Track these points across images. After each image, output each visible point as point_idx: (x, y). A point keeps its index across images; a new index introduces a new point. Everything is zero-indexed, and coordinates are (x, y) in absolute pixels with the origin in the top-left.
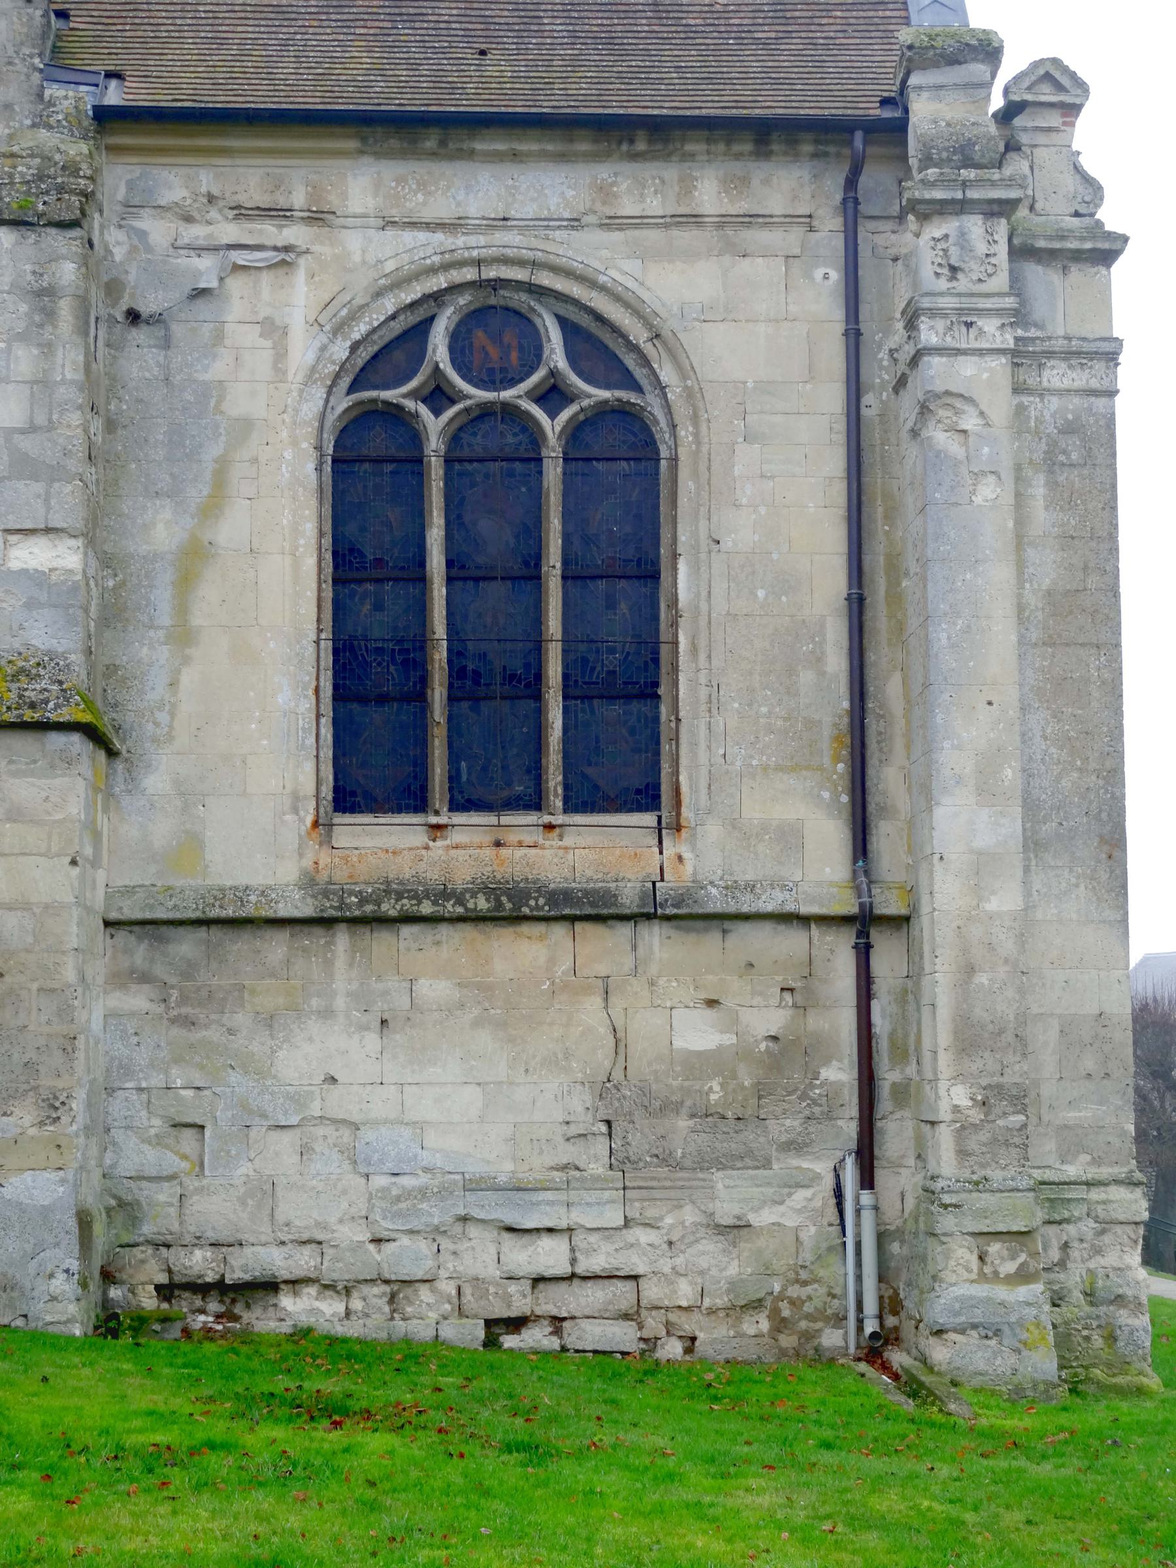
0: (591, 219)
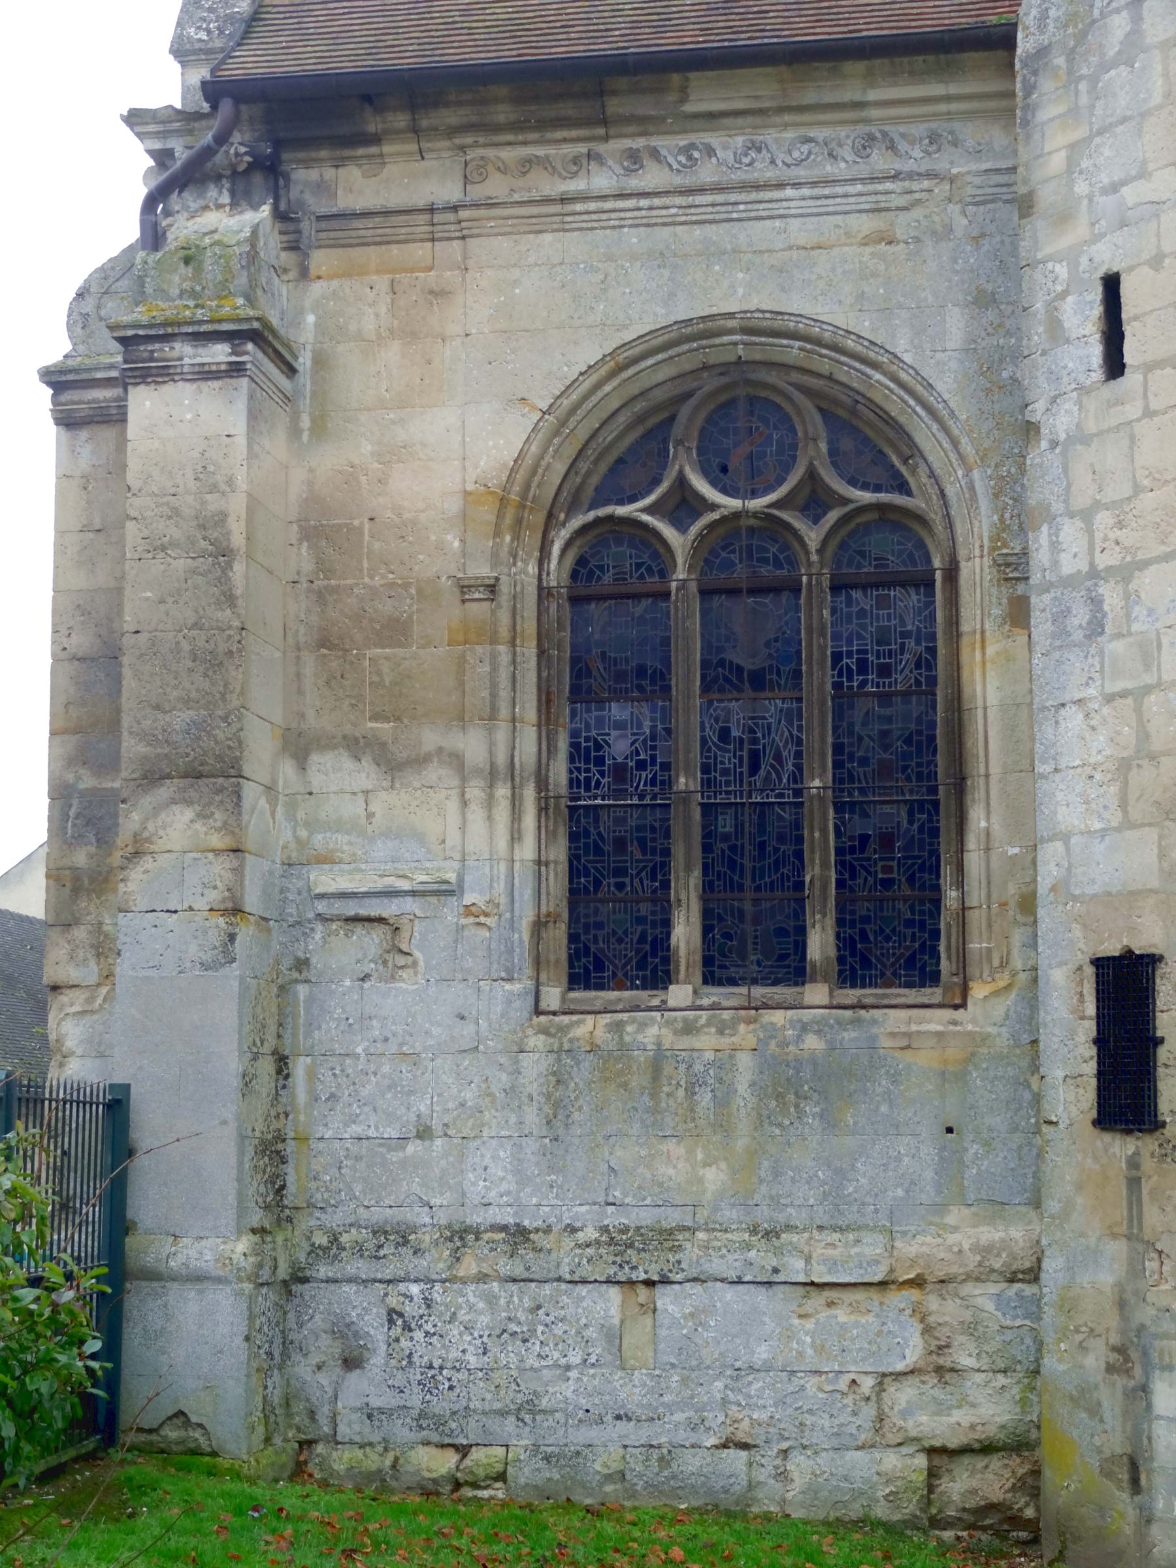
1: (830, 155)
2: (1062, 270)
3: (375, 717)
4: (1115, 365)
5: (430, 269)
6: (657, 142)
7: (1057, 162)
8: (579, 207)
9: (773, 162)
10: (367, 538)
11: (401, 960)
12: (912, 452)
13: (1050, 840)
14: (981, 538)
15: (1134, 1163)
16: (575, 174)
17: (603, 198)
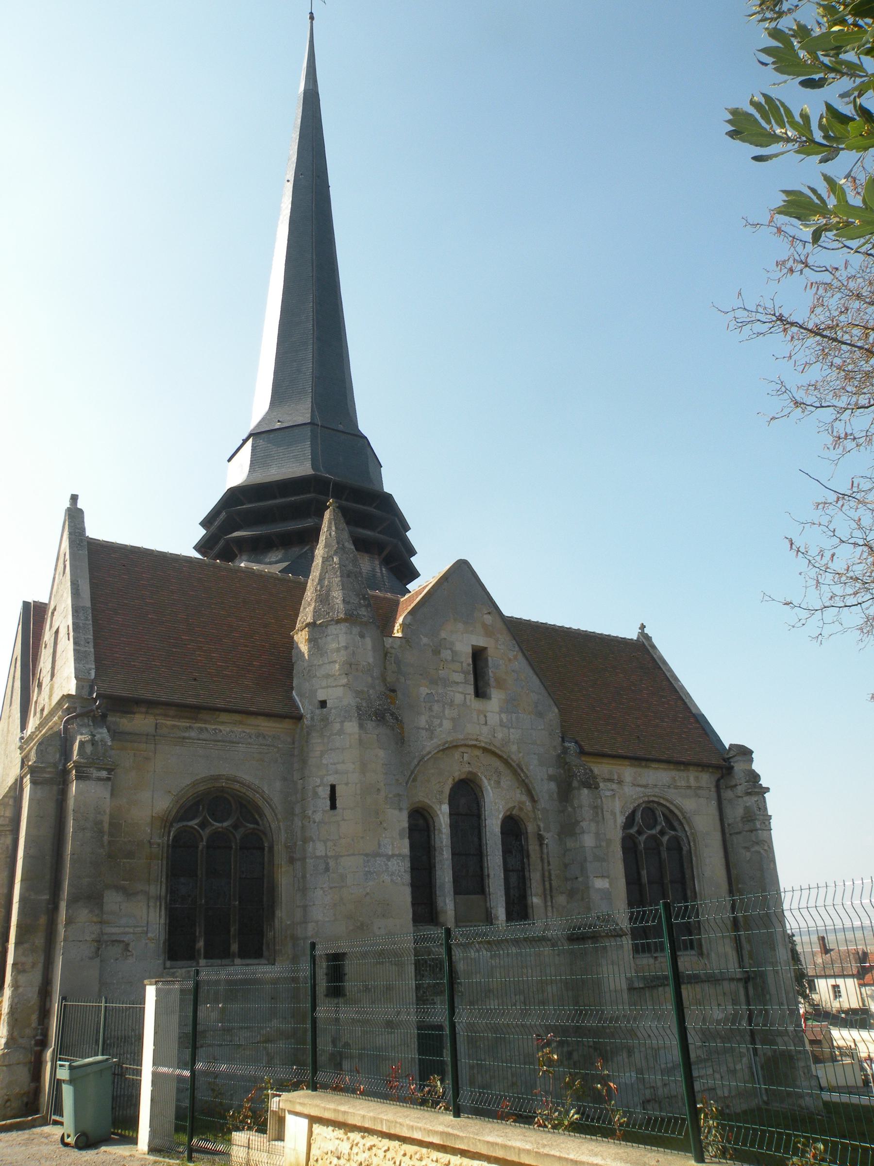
1: (250, 737)
2: (318, 781)
4: (333, 806)
5: (145, 751)
6: (207, 726)
7: (318, 754)
8: (187, 741)
9: (236, 736)
10: (123, 827)
11: (129, 954)
12: (262, 815)
13: (311, 922)
16: (185, 732)
17: (194, 739)
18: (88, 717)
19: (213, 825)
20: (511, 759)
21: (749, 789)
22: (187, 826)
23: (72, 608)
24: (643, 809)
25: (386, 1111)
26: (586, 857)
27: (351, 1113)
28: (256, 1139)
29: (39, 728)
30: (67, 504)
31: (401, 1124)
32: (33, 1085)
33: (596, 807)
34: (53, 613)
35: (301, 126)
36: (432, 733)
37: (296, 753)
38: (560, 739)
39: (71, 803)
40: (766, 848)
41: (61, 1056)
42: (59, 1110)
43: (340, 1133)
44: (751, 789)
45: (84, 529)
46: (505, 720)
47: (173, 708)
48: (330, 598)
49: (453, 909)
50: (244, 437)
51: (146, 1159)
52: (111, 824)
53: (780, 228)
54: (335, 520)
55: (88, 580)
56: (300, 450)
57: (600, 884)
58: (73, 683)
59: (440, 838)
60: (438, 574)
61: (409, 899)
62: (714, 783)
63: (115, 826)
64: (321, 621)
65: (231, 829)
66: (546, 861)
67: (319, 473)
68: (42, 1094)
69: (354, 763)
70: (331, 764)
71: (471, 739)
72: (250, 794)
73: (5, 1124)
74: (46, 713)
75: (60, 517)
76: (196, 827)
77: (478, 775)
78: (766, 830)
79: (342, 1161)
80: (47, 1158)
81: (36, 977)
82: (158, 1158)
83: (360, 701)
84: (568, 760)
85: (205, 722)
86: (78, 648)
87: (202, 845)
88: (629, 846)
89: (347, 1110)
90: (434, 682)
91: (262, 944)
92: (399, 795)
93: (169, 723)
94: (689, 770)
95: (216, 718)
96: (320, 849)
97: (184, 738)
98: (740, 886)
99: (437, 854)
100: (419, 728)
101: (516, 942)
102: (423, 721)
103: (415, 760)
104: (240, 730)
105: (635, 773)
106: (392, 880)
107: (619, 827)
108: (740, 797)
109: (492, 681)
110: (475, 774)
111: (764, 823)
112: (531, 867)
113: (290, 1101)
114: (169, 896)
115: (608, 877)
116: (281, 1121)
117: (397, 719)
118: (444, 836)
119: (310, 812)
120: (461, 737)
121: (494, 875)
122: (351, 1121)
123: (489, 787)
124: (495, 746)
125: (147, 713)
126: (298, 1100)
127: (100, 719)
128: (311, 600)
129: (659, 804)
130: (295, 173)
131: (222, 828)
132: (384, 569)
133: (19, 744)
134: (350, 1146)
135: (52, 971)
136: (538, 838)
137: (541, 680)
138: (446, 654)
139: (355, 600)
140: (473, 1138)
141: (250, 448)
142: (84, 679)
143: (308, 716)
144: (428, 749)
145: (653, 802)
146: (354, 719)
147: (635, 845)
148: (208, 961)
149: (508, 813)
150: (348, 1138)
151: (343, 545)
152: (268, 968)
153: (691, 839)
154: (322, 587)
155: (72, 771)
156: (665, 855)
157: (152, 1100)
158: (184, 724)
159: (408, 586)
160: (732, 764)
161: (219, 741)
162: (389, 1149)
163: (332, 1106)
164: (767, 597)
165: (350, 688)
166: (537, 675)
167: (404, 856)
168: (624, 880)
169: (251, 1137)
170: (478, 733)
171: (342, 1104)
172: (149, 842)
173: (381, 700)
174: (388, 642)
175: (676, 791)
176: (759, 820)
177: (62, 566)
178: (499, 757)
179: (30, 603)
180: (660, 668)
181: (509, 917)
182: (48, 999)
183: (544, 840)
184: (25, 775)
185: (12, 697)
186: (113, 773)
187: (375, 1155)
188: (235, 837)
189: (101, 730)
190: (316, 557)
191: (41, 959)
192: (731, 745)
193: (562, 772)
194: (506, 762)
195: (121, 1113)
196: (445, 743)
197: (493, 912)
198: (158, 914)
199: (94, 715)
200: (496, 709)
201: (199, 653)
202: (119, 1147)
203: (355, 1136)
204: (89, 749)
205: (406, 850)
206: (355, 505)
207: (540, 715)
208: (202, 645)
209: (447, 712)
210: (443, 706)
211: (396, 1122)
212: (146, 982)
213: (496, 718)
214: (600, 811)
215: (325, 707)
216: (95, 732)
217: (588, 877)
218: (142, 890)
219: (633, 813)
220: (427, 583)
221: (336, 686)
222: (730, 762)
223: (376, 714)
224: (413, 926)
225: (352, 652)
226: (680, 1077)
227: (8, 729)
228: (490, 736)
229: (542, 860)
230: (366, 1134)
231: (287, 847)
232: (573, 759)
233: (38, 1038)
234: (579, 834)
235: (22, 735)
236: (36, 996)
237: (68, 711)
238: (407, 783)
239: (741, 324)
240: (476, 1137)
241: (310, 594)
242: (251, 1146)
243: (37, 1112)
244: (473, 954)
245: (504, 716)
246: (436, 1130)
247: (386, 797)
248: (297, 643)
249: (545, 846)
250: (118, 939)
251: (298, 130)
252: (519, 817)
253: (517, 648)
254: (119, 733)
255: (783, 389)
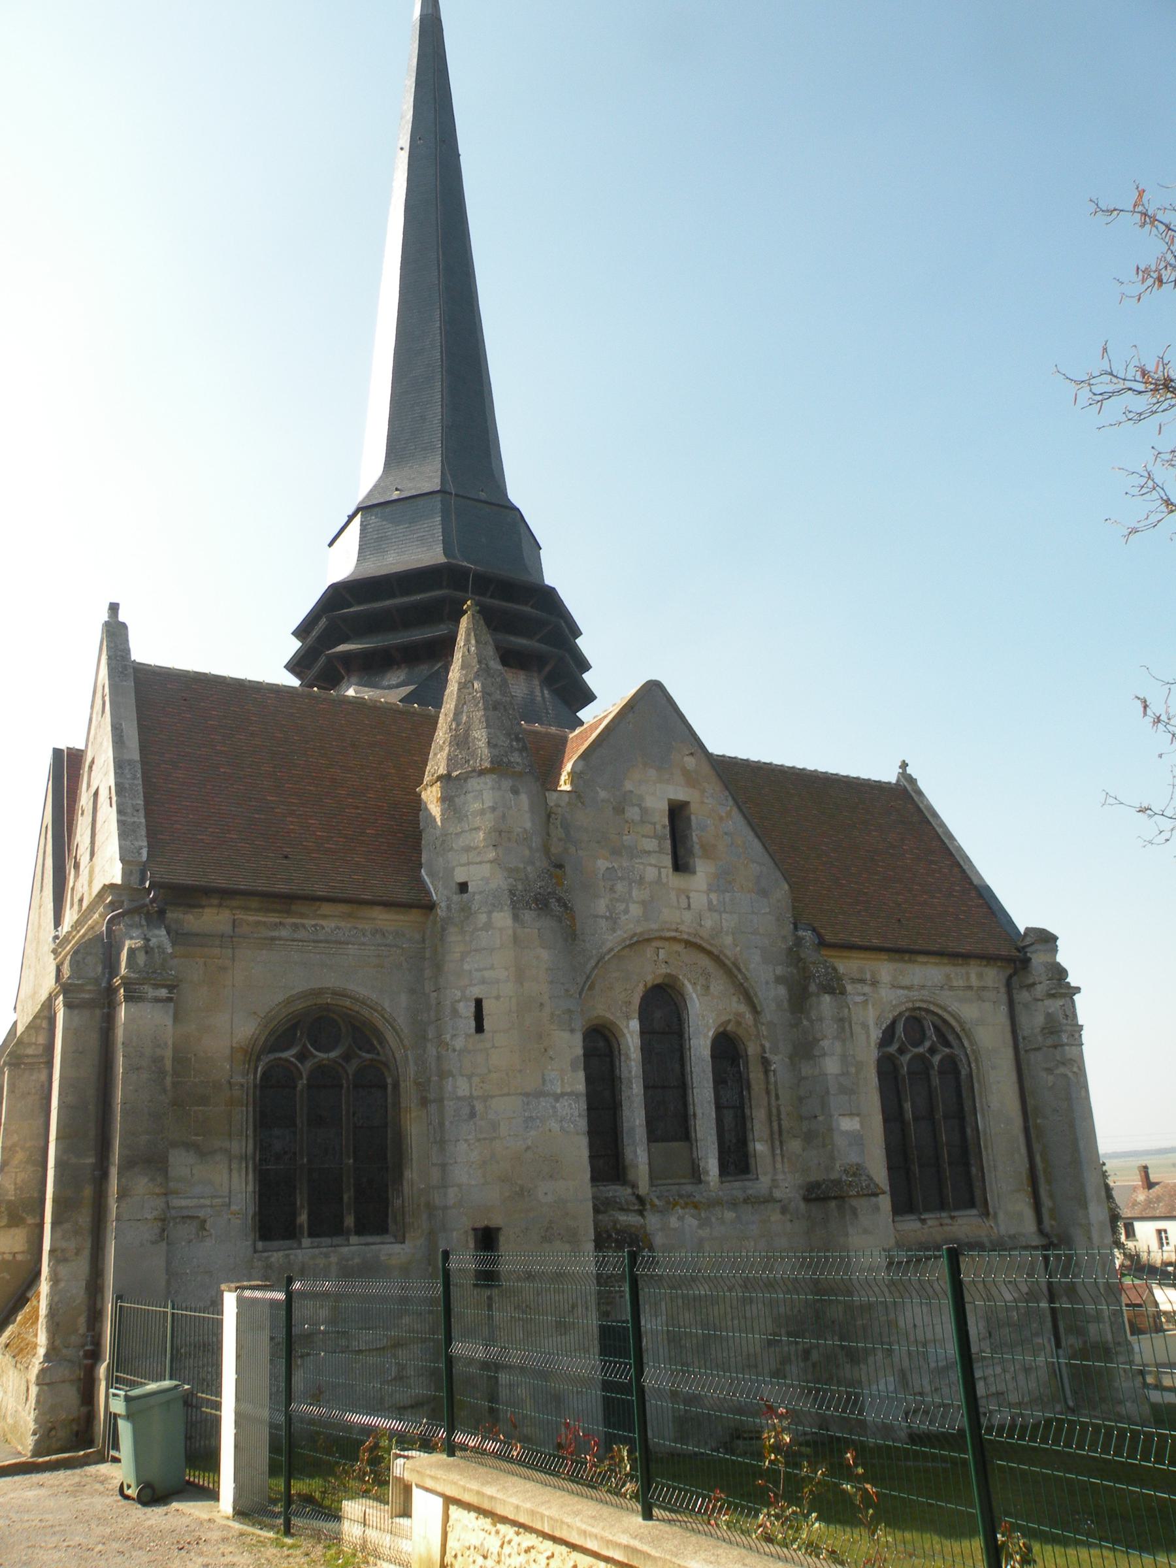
0: (946, 987)
1: (363, 934)
2: (459, 994)
3: (197, 1135)
4: (480, 1028)
5: (219, 959)
6: (305, 921)
9: (344, 934)
11: (205, 1233)
12: (382, 1040)
13: (452, 1186)
14: (410, 1078)
15: (490, 1298)
17: (287, 940)
18: (139, 914)
19: (315, 1056)
20: (725, 955)
21: (1052, 989)
22: (280, 1059)
23: (114, 762)
24: (907, 1019)
25: (549, 1501)
26: (828, 1088)
27: (500, 1500)
28: (375, 1514)
29: (77, 925)
30: (105, 617)
31: (569, 1526)
32: (84, 1410)
33: (842, 1020)
34: (91, 767)
35: (417, 69)
36: (615, 923)
37: (428, 955)
38: (791, 926)
39: (120, 1033)
40: (1075, 1069)
41: (118, 1374)
42: (116, 1446)
43: (486, 1523)
44: (1054, 988)
45: (129, 650)
46: (715, 902)
47: (257, 898)
48: (470, 739)
49: (647, 1161)
50: (350, 513)
51: (229, 1526)
52: (174, 1059)
53: (1155, 215)
54: (475, 630)
55: (136, 722)
56: (427, 529)
57: (848, 1124)
58: (117, 868)
59: (628, 1066)
60: (619, 702)
61: (585, 1153)
62: (1004, 981)
63: (181, 1060)
64: (458, 773)
65: (340, 1061)
66: (773, 1094)
67: (454, 561)
68: (96, 1422)
69: (507, 969)
70: (477, 970)
71: (669, 930)
72: (365, 1012)
73: (50, 1460)
74: (85, 904)
75: (94, 635)
76: (292, 1059)
77: (679, 979)
78: (1076, 1045)
79: (490, 1563)
80: (99, 1519)
81: (82, 1266)
82: (245, 1527)
83: (514, 883)
84: (803, 956)
85: (302, 915)
86: (123, 818)
87: (302, 1083)
88: (887, 1069)
89: (494, 1495)
90: (616, 852)
91: (387, 1215)
92: (570, 1011)
93: (251, 918)
94: (968, 964)
95: (317, 910)
96: (463, 1087)
97: (273, 939)
98: (1038, 1121)
99: (623, 1088)
100: (597, 916)
101: (734, 1204)
102: (601, 906)
103: (592, 961)
104: (349, 925)
105: (895, 970)
106: (562, 1128)
107: (873, 1044)
108: (1039, 1000)
109: (697, 849)
110: (674, 978)
111: (1073, 1035)
112: (753, 1102)
113: (418, 1472)
114: (258, 1155)
115: (858, 1115)
116: (407, 1490)
117: (565, 905)
118: (633, 1063)
119: (448, 1037)
120: (654, 926)
121: (703, 1114)
122: (500, 1511)
123: (694, 996)
124: (701, 938)
125: (220, 905)
126: (428, 1472)
127: (156, 917)
128: (444, 743)
129: (927, 1011)
130: (411, 136)
131: (328, 1059)
132: (546, 692)
133: (53, 946)
134: (499, 1543)
135: (103, 1259)
136: (763, 1064)
137: (764, 845)
138: (633, 813)
139: (503, 741)
140: (671, 1562)
141: (358, 528)
142: (132, 861)
143: (443, 905)
144: (609, 945)
145: (919, 1009)
146: (506, 908)
147: (896, 1068)
148: (314, 1239)
149: (721, 1029)
150: (497, 1532)
151: (486, 664)
152: (397, 1248)
153: (972, 1058)
154: (458, 725)
155: (119, 990)
156: (936, 1081)
157: (236, 1447)
158: (272, 920)
159: (580, 714)
160: (1029, 954)
161: (320, 941)
162: (553, 1555)
163: (474, 1486)
164: (1111, 799)
165: (499, 864)
166: (759, 837)
167: (577, 1095)
168: (881, 1117)
169: (367, 1510)
170: (679, 921)
171: (488, 1483)
172: (230, 1083)
173: (543, 880)
174: (552, 798)
175: (951, 993)
176: (1066, 1031)
177: (101, 702)
178: (709, 953)
179: (62, 751)
180: (929, 822)
181: (724, 1170)
182: (99, 1297)
183: (771, 1066)
184: (57, 996)
185: (42, 879)
186: (175, 991)
187: (534, 1561)
188: (346, 1072)
189: (157, 932)
190: (449, 682)
191: (88, 1244)
192: (1027, 929)
193: (795, 971)
194: (717, 959)
195: (202, 1443)
196: (632, 937)
197: (702, 1164)
198: (244, 1179)
199: (148, 912)
200: (704, 886)
201: (291, 819)
202: (195, 1503)
203: (507, 1531)
204: (141, 959)
205: (581, 1087)
206: (504, 604)
207: (764, 893)
208: (295, 808)
209: (635, 893)
210: (630, 884)
211: (562, 1522)
212: (223, 1287)
213: (704, 899)
214: (847, 1025)
215: (467, 891)
216: (149, 935)
217: (831, 1116)
218: (221, 1148)
219: (893, 1023)
220: (605, 713)
221: (481, 863)
222: (1026, 952)
223: (536, 900)
224: (592, 1186)
225: (501, 814)
226: (956, 1375)
227: (39, 923)
228: (695, 925)
229: (768, 1092)
230: (521, 1530)
231: (418, 1084)
232: (808, 953)
233: (88, 1348)
234: (819, 1057)
235: (57, 933)
236: (82, 1292)
237: (112, 906)
238: (580, 994)
239: (1100, 398)
240: (674, 1560)
241: (442, 734)
242: (367, 1523)
243: (90, 1443)
244: (674, 1222)
245: (713, 896)
246: (619, 1541)
247: (552, 1014)
248: (426, 803)
249: (772, 1073)
250: (190, 1214)
251: (414, 74)
252: (737, 1035)
253: (731, 802)
254: (183, 934)
255: (1150, 484)
